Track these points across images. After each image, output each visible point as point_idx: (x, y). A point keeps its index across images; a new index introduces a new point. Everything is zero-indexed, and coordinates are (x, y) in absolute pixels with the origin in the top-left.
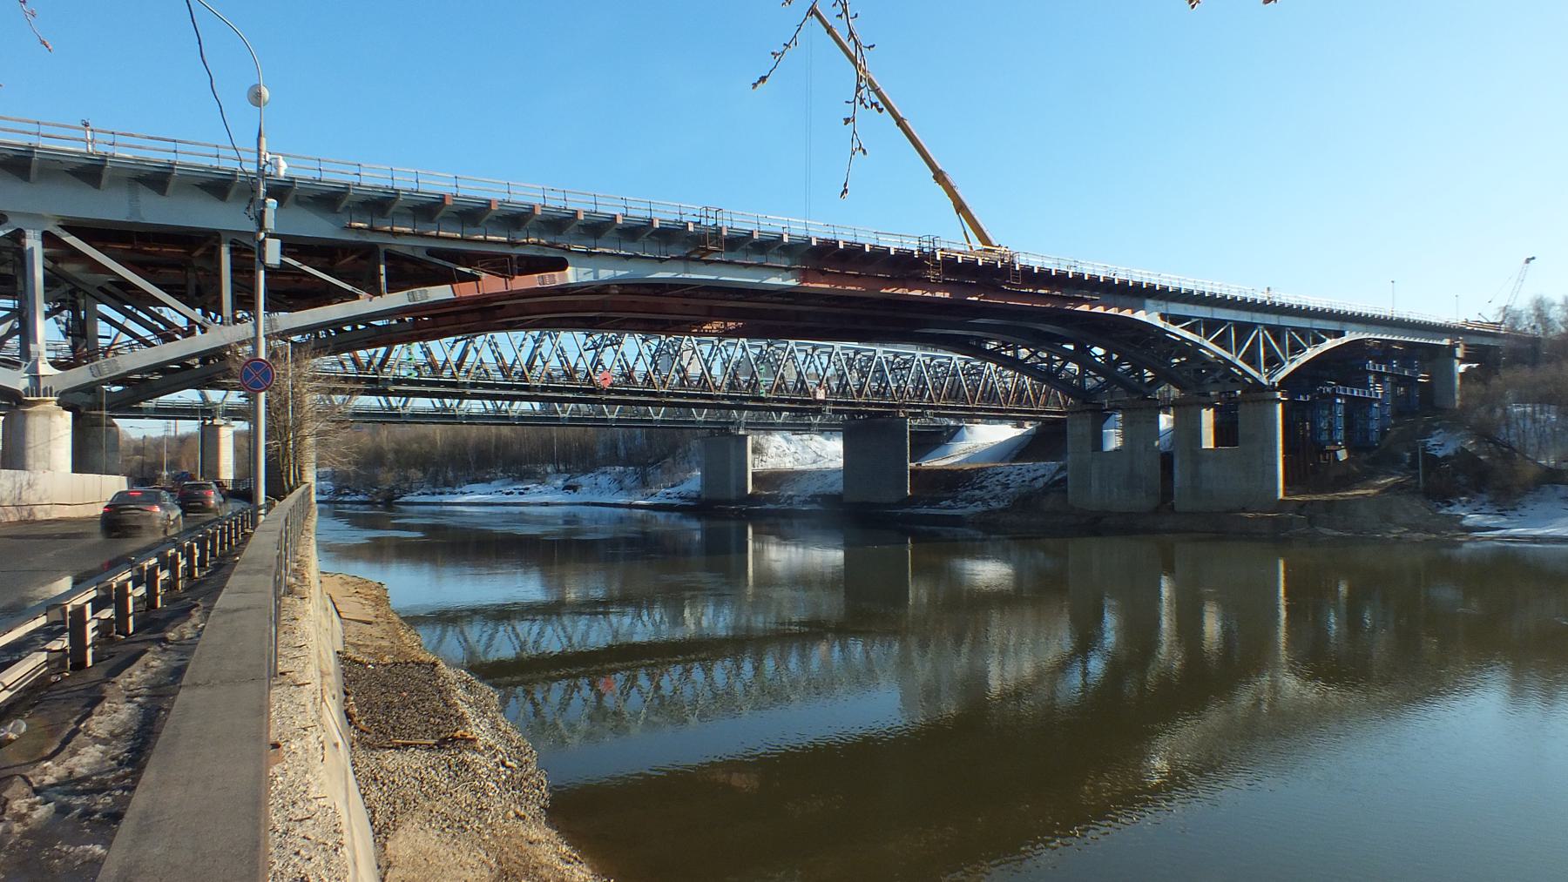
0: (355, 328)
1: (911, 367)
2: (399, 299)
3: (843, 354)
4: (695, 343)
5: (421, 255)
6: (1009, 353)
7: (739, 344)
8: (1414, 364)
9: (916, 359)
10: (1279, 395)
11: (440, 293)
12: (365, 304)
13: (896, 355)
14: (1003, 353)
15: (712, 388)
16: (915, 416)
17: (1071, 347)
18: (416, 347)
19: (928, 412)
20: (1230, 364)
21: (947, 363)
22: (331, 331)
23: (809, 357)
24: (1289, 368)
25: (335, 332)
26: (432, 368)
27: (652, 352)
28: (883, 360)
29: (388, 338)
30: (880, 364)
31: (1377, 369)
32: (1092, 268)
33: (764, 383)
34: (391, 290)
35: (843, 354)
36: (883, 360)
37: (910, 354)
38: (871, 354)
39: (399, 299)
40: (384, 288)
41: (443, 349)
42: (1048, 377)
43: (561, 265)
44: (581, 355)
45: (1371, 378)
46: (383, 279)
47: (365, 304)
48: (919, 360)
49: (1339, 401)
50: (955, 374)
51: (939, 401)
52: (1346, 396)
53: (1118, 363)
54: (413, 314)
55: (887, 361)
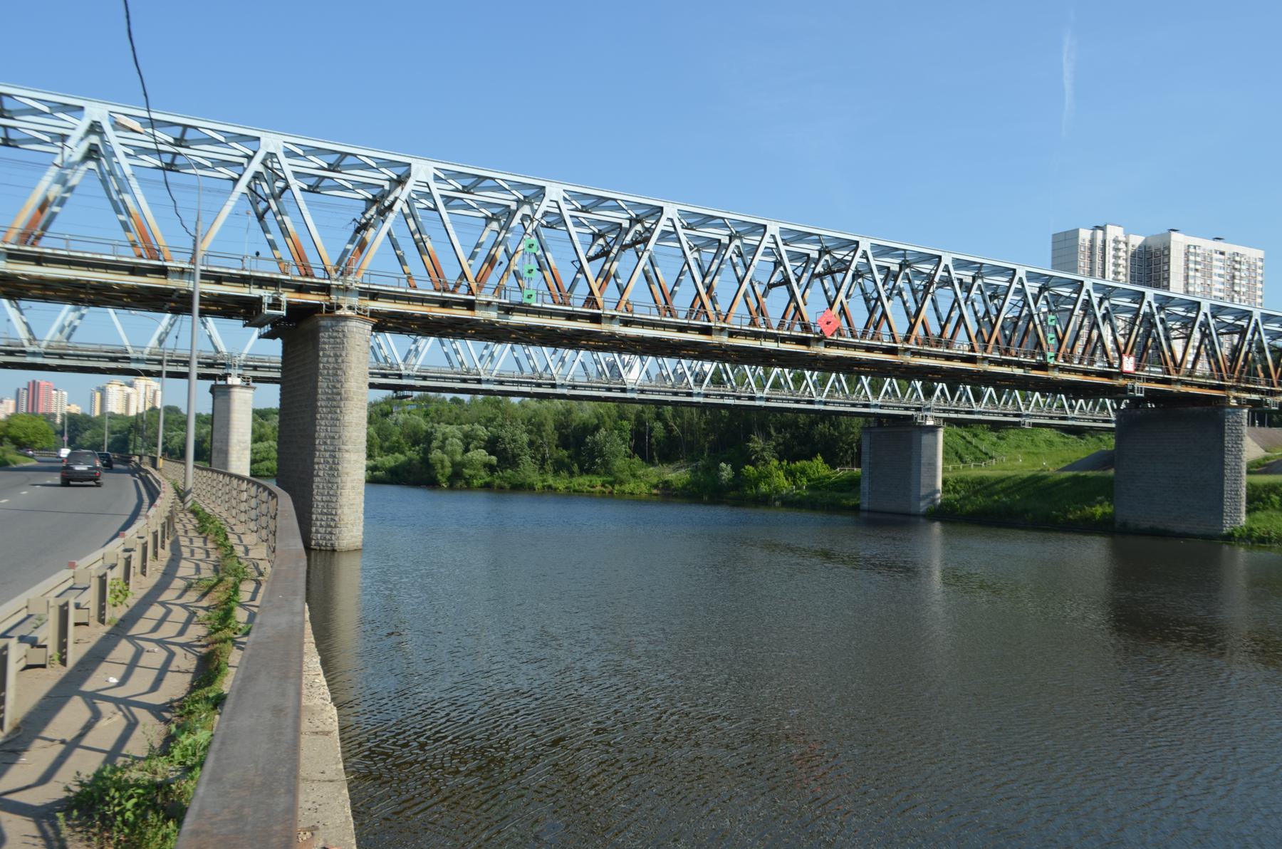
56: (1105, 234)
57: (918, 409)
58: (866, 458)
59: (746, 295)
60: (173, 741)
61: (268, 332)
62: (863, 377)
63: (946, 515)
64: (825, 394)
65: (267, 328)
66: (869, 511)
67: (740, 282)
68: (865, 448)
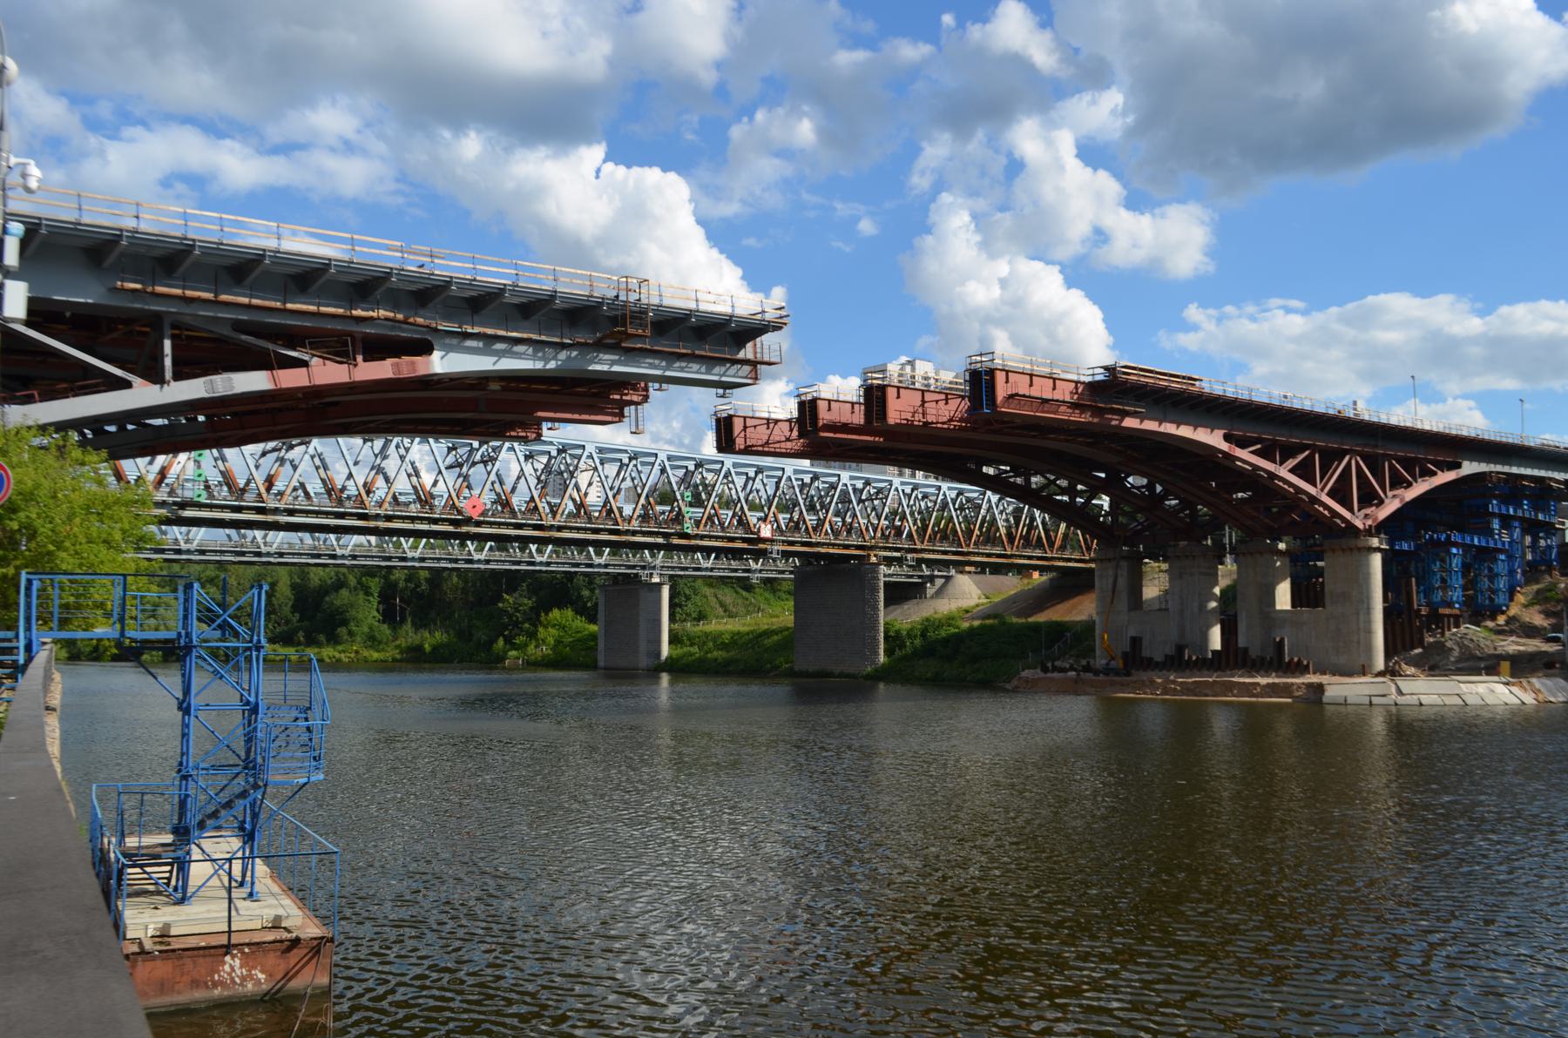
0: (122, 428)
1: (886, 498)
2: (193, 389)
3: (797, 479)
4: (597, 461)
5: (226, 331)
6: (1019, 480)
7: (657, 464)
8: (1549, 506)
9: (893, 488)
10: (1375, 542)
11: (254, 381)
12: (142, 394)
13: (867, 483)
14: (1012, 480)
15: (619, 520)
16: (889, 561)
17: (1103, 475)
18: (208, 456)
19: (909, 556)
20: (1314, 500)
21: (933, 494)
22: (86, 431)
23: (751, 482)
24: (1391, 506)
25: (94, 435)
26: (230, 488)
27: (538, 474)
28: (850, 488)
29: (170, 442)
30: (845, 493)
31: (1504, 512)
32: (514, 272)
33: (690, 515)
34: (178, 376)
35: (797, 479)
36: (850, 488)
37: (834, 475)
38: (834, 479)
39: (193, 389)
40: (168, 374)
41: (244, 460)
42: (1082, 517)
43: (425, 349)
44: (440, 472)
45: (1496, 525)
46: (168, 362)
47: (142, 394)
48: (897, 490)
49: (1454, 551)
50: (945, 505)
51: (923, 543)
52: (1464, 546)
53: (1165, 495)
54: (210, 412)
55: (855, 490)
56: (913, 369)
57: (643, 568)
58: (601, 615)
59: (493, 483)
60: (123, 643)
61: (543, 657)
62: (469, 543)
63: (677, 668)
64: (546, 555)
65: (601, 1024)
66: (605, 669)
67: (489, 473)
68: (601, 608)
